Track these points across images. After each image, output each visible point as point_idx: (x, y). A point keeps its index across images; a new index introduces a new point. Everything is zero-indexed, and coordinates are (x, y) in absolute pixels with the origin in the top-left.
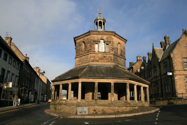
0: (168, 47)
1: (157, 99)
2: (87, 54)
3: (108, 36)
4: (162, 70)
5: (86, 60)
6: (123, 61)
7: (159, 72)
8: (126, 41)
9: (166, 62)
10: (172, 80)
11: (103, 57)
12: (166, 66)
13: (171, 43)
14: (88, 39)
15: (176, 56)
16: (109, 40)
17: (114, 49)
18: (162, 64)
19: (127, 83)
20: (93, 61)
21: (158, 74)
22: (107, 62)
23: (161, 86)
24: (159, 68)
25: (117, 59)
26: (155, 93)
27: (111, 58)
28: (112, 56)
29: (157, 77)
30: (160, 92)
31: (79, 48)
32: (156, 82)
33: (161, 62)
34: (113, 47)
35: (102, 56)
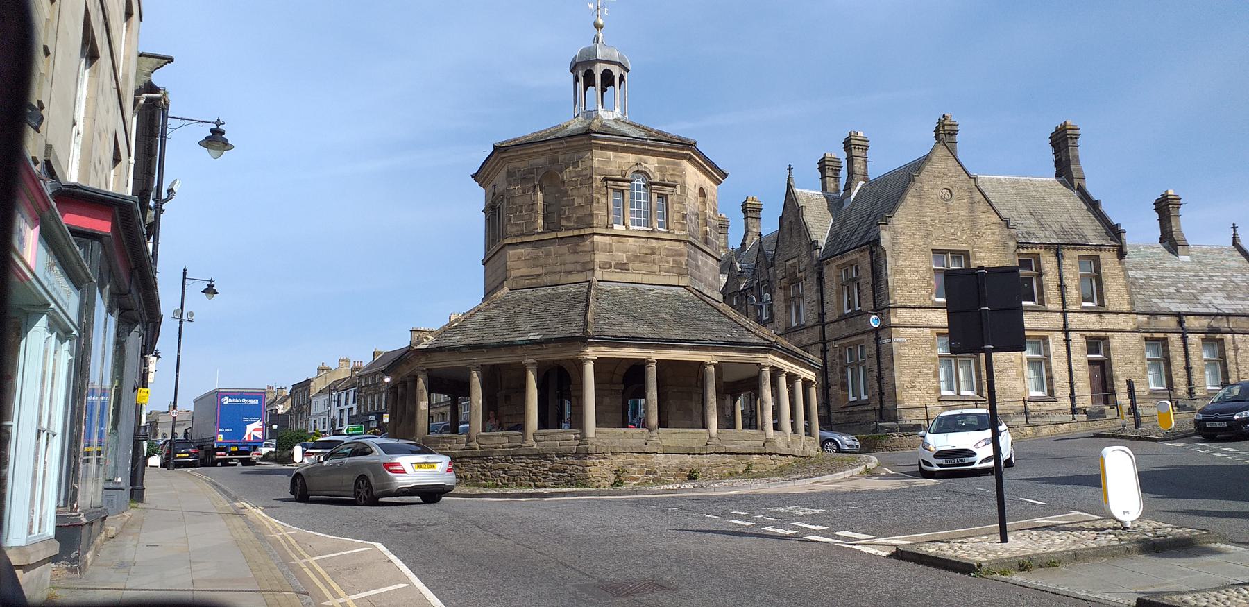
2: (576, 233)
4: (830, 296)
7: (816, 309)
11: (644, 251)
15: (904, 244)
21: (808, 315)
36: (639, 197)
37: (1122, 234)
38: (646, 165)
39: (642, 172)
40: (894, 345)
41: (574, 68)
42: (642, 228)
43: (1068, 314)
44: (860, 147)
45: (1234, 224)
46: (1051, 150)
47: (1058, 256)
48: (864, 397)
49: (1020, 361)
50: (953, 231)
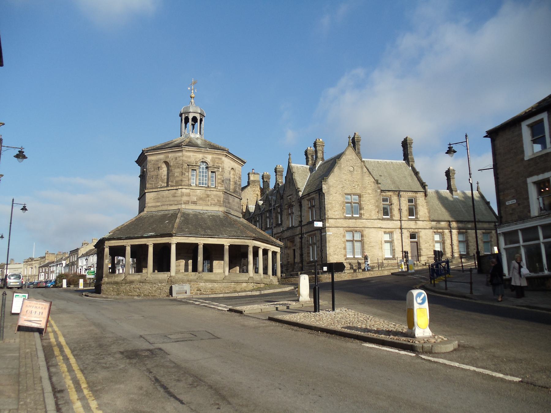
0: (321, 165)
1: (291, 275)
2: (175, 188)
3: (215, 156)
5: (172, 199)
6: (238, 203)
8: (245, 163)
9: (313, 199)
10: (321, 236)
12: (314, 206)
13: (326, 158)
14: (176, 158)
15: (332, 190)
16: (216, 164)
17: (225, 181)
18: (305, 204)
19: (249, 245)
20: (187, 203)
21: (295, 223)
22: (211, 205)
23: (301, 248)
24: (298, 209)
25: (228, 200)
26: (288, 262)
27: (220, 197)
28: (221, 194)
29: (293, 227)
30: (297, 259)
31: (155, 173)
32: (291, 239)
33: (303, 197)
34: (223, 179)
35: (203, 194)
36: (203, 172)
37: (426, 187)
38: (206, 159)
39: (205, 162)
40: (327, 236)
41: (181, 115)
42: (204, 186)
43: (402, 221)
44: (320, 146)
45: (478, 182)
46: (402, 148)
47: (399, 196)
48: (316, 259)
49: (381, 242)
50: (354, 185)
